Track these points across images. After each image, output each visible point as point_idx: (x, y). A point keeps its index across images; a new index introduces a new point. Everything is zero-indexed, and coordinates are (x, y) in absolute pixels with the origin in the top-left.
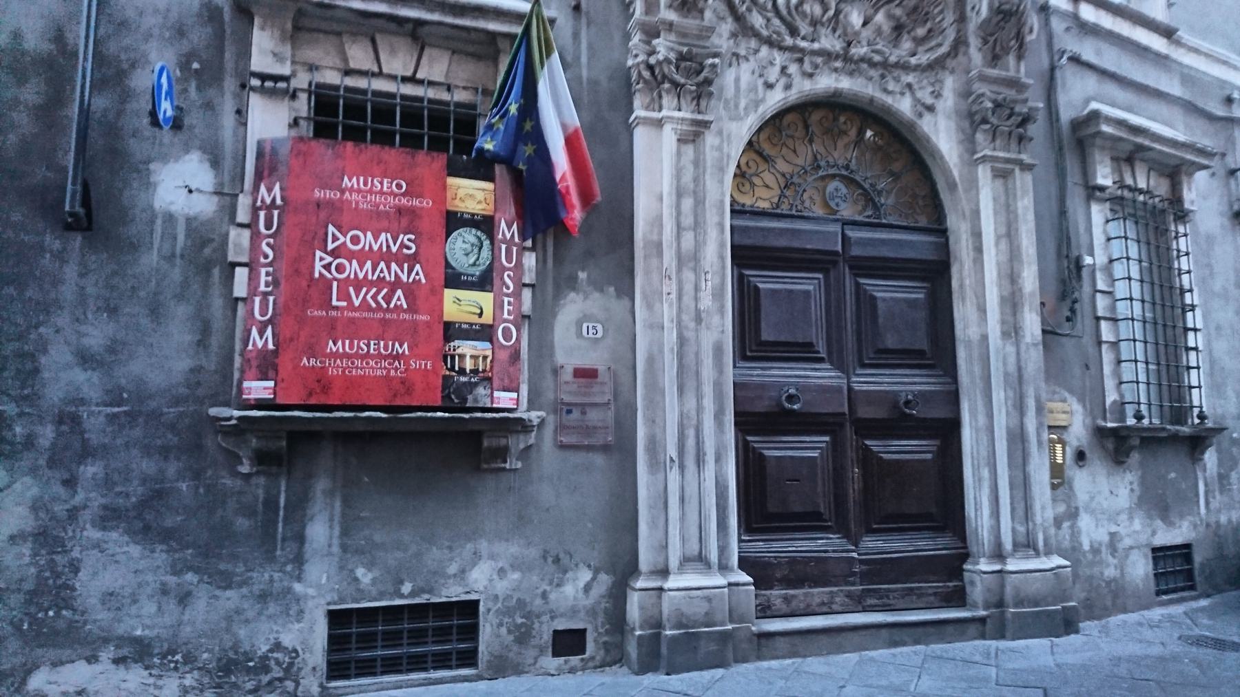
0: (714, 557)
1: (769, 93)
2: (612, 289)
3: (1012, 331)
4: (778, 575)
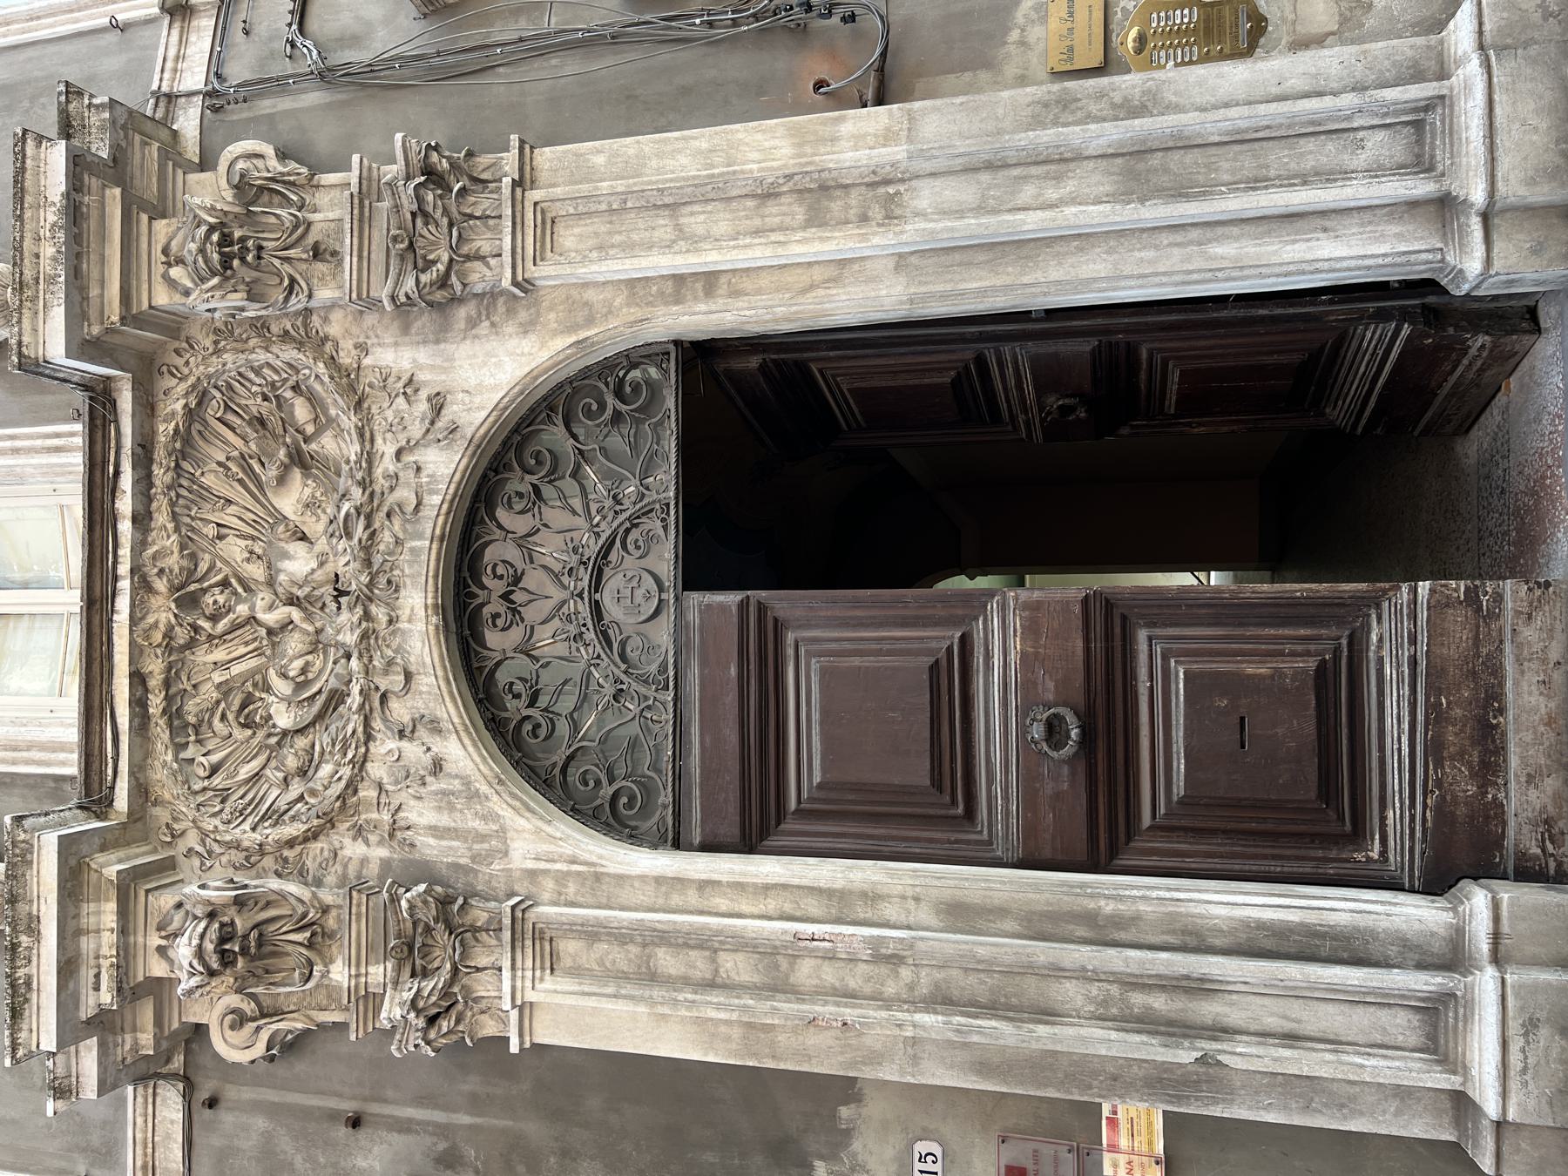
0: (1425, 982)
2: (844, 1112)
3: (883, 192)
4: (1472, 789)
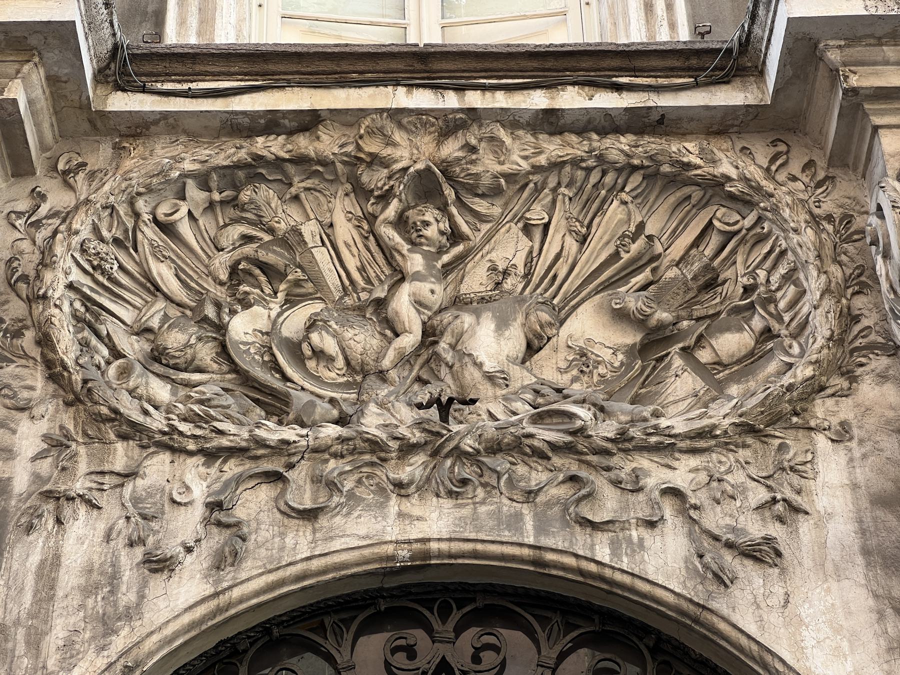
1: (157, 583)
